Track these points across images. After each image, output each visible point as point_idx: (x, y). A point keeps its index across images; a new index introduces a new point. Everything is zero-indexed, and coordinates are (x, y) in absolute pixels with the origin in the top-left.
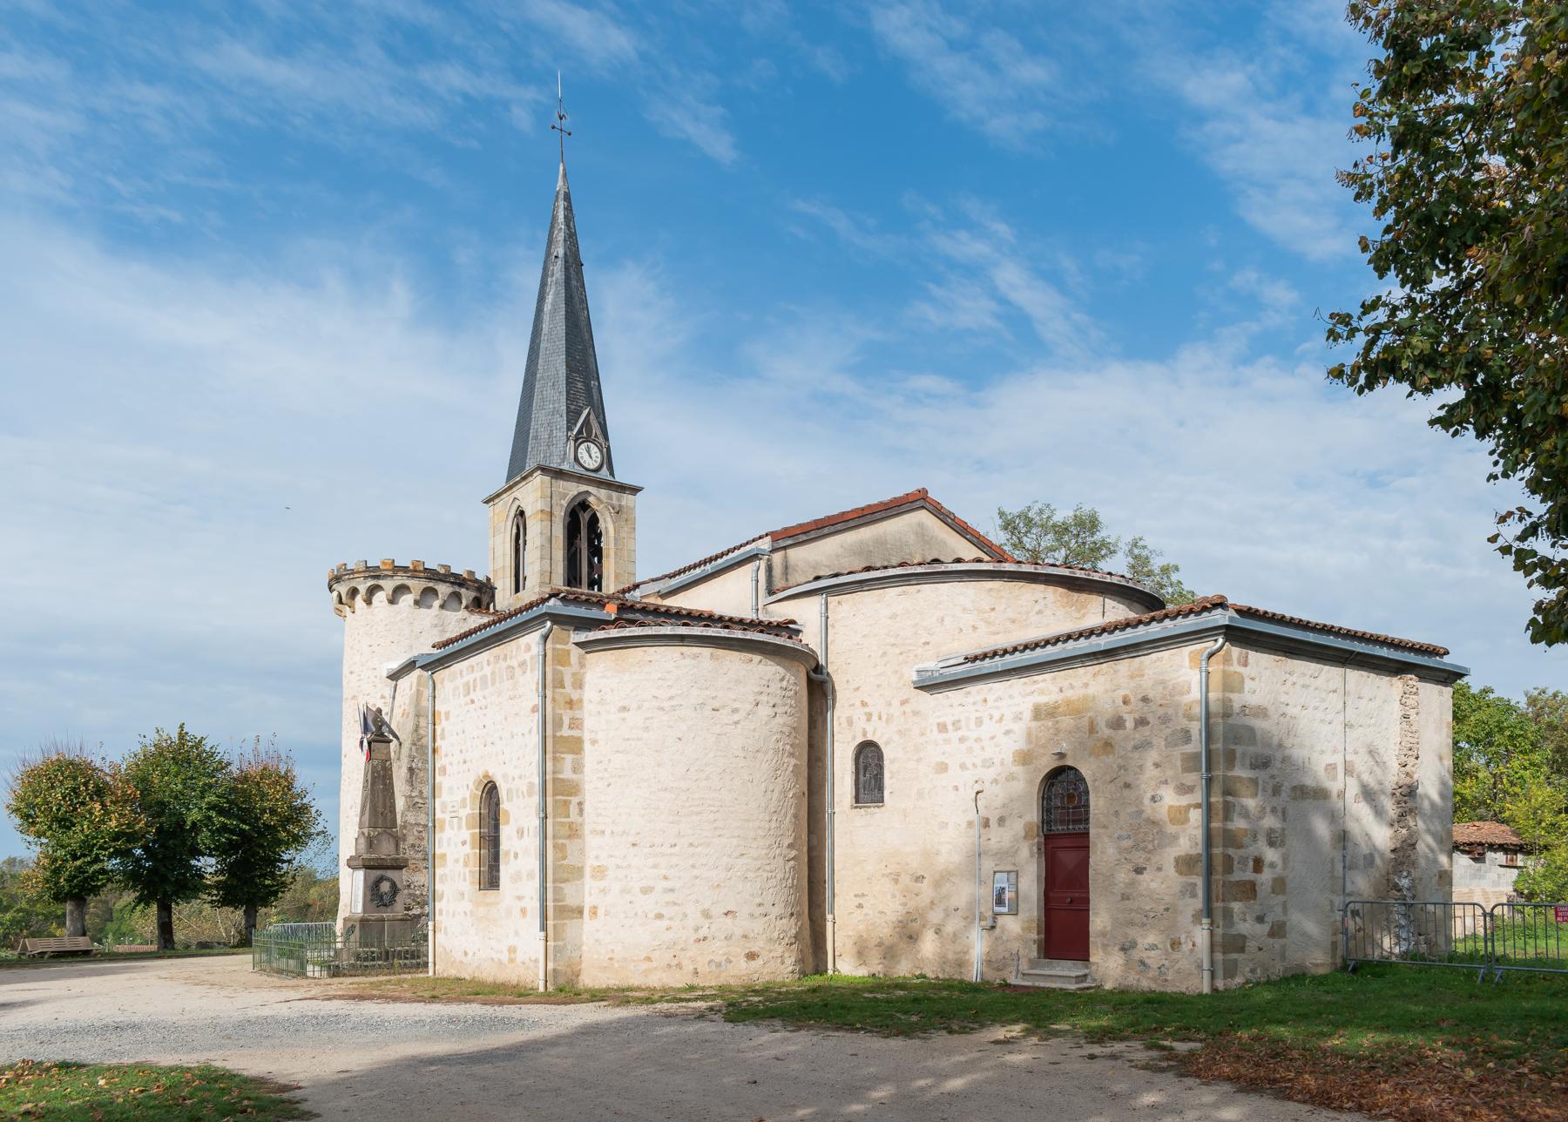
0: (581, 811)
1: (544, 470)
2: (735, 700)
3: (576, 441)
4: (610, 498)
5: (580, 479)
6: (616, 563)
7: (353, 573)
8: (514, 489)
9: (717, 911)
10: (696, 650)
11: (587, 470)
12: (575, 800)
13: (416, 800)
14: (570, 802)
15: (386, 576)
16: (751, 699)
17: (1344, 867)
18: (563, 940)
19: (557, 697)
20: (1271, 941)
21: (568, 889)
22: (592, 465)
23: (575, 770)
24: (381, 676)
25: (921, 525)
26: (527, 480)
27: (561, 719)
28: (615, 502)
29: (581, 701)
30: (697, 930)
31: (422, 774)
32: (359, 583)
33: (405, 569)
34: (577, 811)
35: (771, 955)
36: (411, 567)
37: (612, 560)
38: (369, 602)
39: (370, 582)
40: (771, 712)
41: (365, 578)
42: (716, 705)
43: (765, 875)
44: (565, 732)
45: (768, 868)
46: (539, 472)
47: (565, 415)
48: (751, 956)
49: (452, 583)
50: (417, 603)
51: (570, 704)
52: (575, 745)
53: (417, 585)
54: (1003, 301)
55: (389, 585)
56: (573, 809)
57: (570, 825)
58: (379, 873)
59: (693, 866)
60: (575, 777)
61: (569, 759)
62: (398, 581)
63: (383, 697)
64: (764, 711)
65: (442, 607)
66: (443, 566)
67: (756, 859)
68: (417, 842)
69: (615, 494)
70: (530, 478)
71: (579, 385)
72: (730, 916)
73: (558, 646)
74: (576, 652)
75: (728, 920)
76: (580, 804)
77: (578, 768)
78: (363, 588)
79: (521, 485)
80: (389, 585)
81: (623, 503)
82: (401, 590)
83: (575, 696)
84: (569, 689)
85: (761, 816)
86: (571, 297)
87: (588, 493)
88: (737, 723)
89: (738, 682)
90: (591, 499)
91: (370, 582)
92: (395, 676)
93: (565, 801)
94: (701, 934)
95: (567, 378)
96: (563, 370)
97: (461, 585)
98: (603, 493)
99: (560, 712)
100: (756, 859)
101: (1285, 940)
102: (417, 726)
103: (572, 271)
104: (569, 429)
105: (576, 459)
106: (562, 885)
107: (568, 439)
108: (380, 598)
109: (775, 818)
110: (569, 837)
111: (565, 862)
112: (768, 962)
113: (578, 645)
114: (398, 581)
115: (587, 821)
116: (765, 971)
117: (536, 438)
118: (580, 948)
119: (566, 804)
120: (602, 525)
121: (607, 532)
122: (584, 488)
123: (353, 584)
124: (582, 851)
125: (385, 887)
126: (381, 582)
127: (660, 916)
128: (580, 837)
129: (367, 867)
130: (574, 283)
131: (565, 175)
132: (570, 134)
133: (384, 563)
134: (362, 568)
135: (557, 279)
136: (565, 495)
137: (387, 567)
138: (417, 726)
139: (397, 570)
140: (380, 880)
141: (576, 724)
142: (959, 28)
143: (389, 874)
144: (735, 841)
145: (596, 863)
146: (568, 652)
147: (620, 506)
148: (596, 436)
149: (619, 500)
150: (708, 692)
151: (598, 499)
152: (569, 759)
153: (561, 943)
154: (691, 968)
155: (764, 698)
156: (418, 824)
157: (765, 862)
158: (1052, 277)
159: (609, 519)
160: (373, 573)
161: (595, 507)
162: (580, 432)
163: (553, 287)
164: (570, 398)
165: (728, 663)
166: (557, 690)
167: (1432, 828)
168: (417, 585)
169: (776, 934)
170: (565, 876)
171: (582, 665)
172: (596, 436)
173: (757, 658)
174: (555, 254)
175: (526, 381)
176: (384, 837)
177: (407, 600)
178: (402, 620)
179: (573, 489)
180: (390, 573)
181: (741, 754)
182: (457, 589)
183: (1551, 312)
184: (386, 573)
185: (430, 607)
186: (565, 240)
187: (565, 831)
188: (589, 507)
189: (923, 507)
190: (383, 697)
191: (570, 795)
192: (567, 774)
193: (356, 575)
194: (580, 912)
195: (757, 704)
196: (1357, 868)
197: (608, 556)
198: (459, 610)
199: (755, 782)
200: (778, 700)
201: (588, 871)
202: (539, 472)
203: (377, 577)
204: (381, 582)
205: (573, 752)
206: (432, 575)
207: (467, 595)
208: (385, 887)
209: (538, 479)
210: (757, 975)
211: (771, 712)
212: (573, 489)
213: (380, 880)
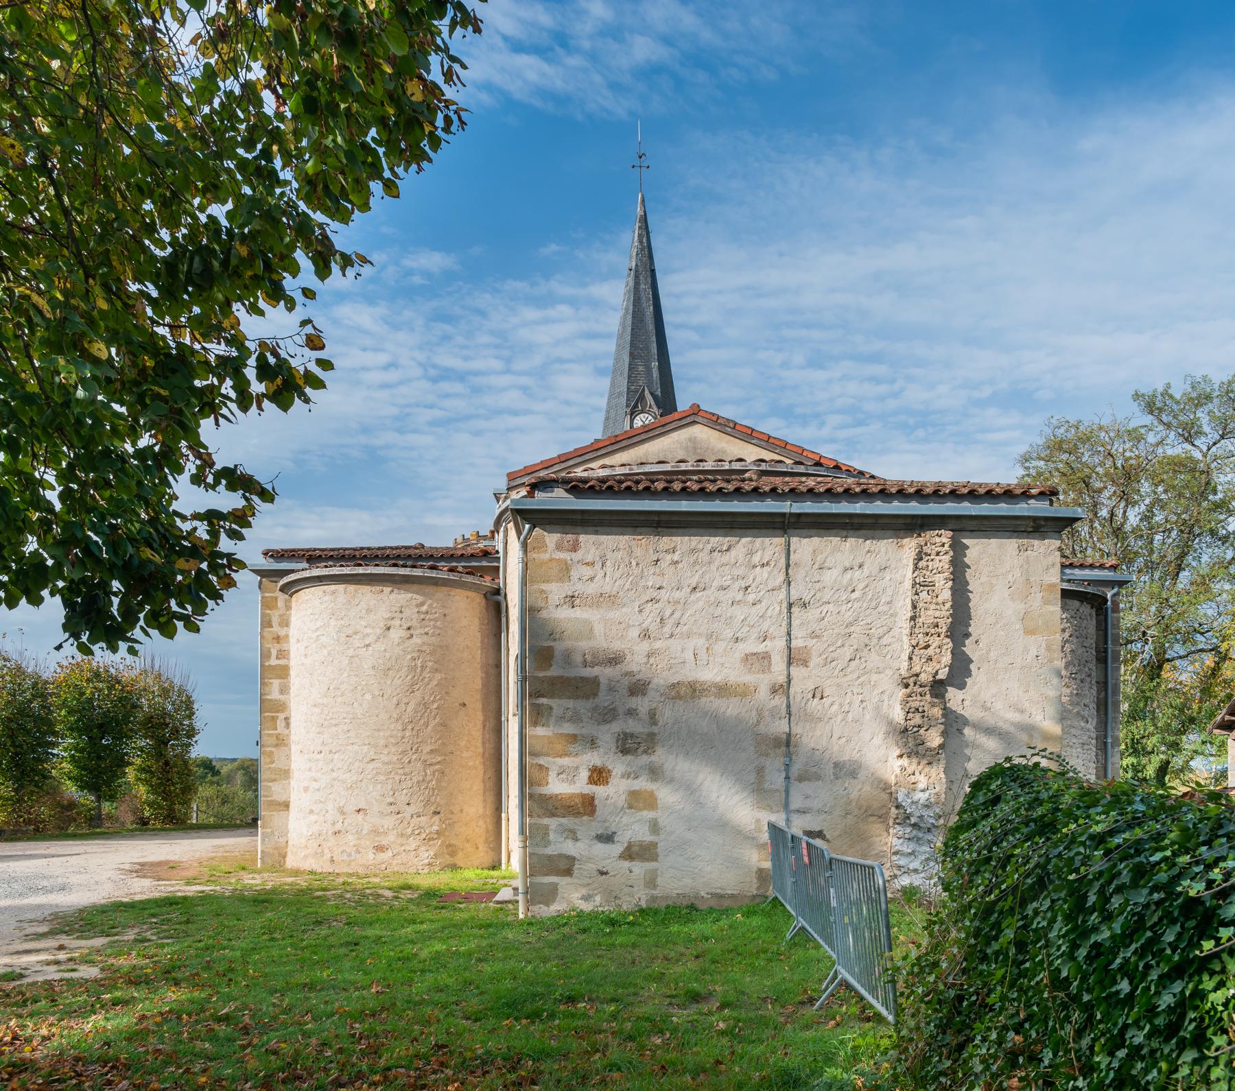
0: (288, 725)
2: (366, 627)
3: (631, 415)
9: (351, 808)
10: (333, 587)
12: (281, 716)
14: (277, 717)
16: (382, 624)
17: (787, 778)
18: (271, 828)
19: (265, 634)
20: (626, 864)
23: (282, 692)
25: (693, 440)
27: (270, 652)
29: (287, 636)
30: (334, 824)
34: (284, 724)
35: (403, 848)
40: (405, 634)
42: (350, 632)
43: (397, 778)
44: (273, 662)
45: (401, 771)
48: (380, 849)
51: (278, 639)
52: (283, 672)
56: (280, 724)
57: (278, 736)
59: (333, 770)
60: (282, 697)
61: (276, 683)
64: (396, 634)
67: (387, 763)
71: (641, 368)
72: (361, 813)
73: (267, 595)
74: (282, 597)
75: (360, 816)
76: (287, 719)
77: (284, 690)
83: (282, 632)
84: (276, 628)
85: (392, 726)
86: (639, 299)
88: (368, 645)
89: (369, 611)
93: (273, 717)
94: (338, 826)
95: (630, 364)
99: (268, 646)
100: (387, 763)
101: (654, 864)
103: (641, 278)
106: (270, 784)
109: (410, 727)
110: (277, 745)
111: (273, 765)
112: (398, 854)
113: (283, 589)
115: (293, 731)
116: (395, 862)
118: (286, 835)
119: (274, 719)
124: (288, 757)
127: (311, 812)
128: (286, 745)
131: (643, 201)
141: (283, 654)
144: (366, 748)
146: (276, 599)
148: (650, 407)
150: (343, 622)
152: (276, 683)
153: (269, 830)
154: (329, 856)
155: (397, 622)
157: (397, 766)
165: (360, 595)
166: (266, 629)
169: (409, 831)
170: (273, 777)
171: (288, 608)
172: (650, 407)
173: (387, 590)
181: (372, 673)
183: (312, 43)
186: (637, 254)
187: (273, 741)
189: (695, 422)
191: (278, 711)
192: (274, 694)
194: (286, 806)
195: (389, 629)
196: (818, 777)
199: (385, 697)
200: (414, 623)
205: (280, 677)
210: (384, 866)
211: (405, 634)
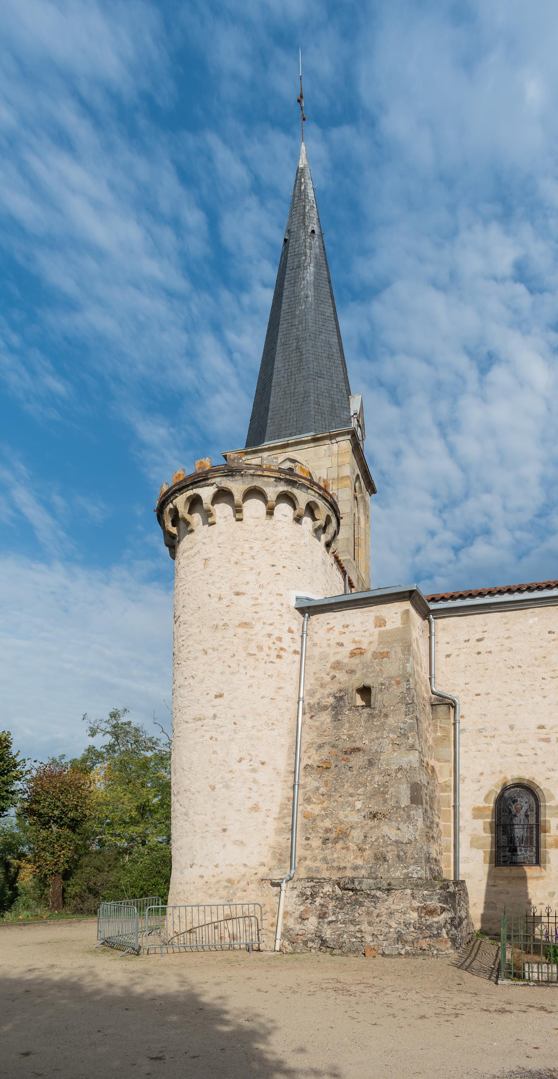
7: (263, 470)
8: (290, 449)
15: (303, 485)
24: (289, 607)
26: (321, 443)
32: (268, 484)
39: (283, 488)
41: (278, 479)
46: (349, 437)
54: (17, 511)
63: (290, 631)
70: (328, 442)
79: (306, 446)
80: (303, 497)
91: (283, 488)
123: (258, 483)
126: (296, 492)
135: (316, 255)
137: (304, 475)
142: (15, 340)
158: (49, 507)
180: (307, 483)
184: (303, 481)
193: (266, 473)
202: (349, 437)
204: (296, 492)
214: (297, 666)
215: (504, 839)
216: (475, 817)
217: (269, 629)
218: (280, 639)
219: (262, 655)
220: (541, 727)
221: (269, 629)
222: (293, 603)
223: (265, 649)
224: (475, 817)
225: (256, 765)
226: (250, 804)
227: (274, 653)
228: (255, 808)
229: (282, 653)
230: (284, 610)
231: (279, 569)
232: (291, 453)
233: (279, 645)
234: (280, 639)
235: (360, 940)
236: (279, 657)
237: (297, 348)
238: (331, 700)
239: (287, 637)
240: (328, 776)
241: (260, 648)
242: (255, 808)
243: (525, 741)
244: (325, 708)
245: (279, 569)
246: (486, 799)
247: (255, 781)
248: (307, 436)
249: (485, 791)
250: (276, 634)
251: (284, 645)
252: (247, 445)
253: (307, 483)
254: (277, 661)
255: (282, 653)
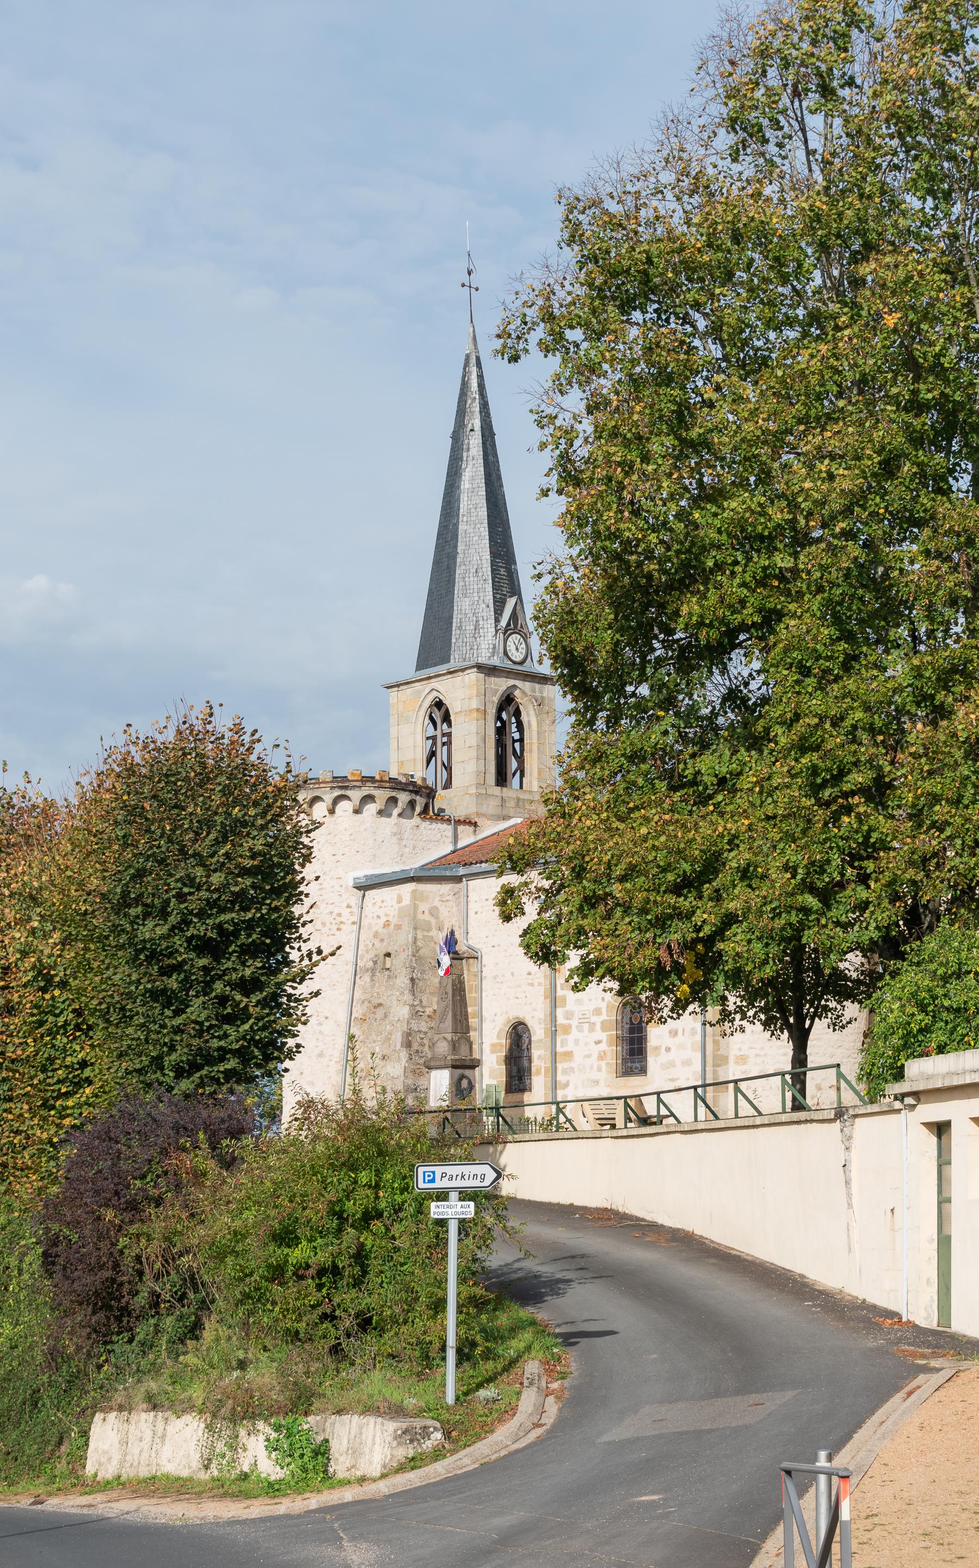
1: (480, 667)
4: (533, 690)
5: (509, 674)
6: (539, 758)
11: (514, 663)
13: (418, 1008)
21: (720, 1071)
22: (518, 657)
24: (347, 888)
28: (537, 694)
31: (421, 984)
32: (325, 793)
33: (372, 779)
36: (378, 778)
37: (535, 755)
38: (332, 811)
41: (332, 788)
47: (491, 606)
49: (411, 791)
50: (380, 813)
53: (382, 795)
55: (356, 795)
58: (460, 1071)
62: (365, 791)
63: (349, 906)
65: (400, 815)
66: (405, 775)
68: (420, 1048)
69: (537, 686)
71: (502, 571)
78: (329, 797)
80: (356, 795)
81: (545, 695)
82: (369, 798)
87: (515, 687)
90: (517, 693)
91: (337, 793)
92: (364, 887)
95: (492, 565)
96: (487, 556)
97: (416, 793)
98: (527, 686)
102: (415, 939)
104: (497, 620)
105: (506, 653)
107: (497, 631)
108: (345, 807)
114: (365, 791)
117: (460, 628)
120: (524, 718)
121: (530, 725)
122: (511, 682)
123: (317, 793)
125: (465, 1083)
126: (348, 793)
129: (454, 1067)
130: (491, 458)
132: (477, 289)
133: (353, 774)
134: (329, 778)
136: (496, 691)
138: (415, 939)
139: (367, 780)
140: (462, 1077)
143: (467, 1072)
145: (739, 1053)
147: (542, 698)
149: (541, 692)
151: (523, 692)
156: (420, 1031)
159: (532, 713)
160: (341, 783)
161: (519, 700)
162: (509, 624)
163: (471, 463)
164: (496, 588)
167: (738, 933)
168: (382, 795)
174: (470, 427)
175: (437, 563)
176: (463, 1041)
177: (371, 808)
178: (366, 830)
179: (501, 685)
180: (358, 784)
182: (414, 796)
185: (389, 816)
188: (513, 700)
190: (349, 906)
197: (531, 751)
198: (412, 817)
201: (732, 1060)
203: (346, 788)
204: (348, 793)
206: (396, 784)
207: (420, 802)
208: (465, 1083)
209: (473, 676)
212: (501, 685)
213: (462, 1077)
214: (354, 935)
215: (515, 1069)
216: (493, 1052)
217: (331, 908)
218: (340, 915)
219: (325, 930)
220: (529, 974)
221: (331, 908)
222: (351, 883)
223: (328, 925)
224: (493, 1052)
225: (322, 1019)
226: (317, 1052)
227: (335, 927)
228: (321, 1055)
229: (342, 926)
230: (342, 890)
231: (339, 857)
232: (434, 684)
233: (339, 919)
234: (340, 915)
235: (561, 1116)
236: (339, 929)
237: (448, 567)
238: (371, 964)
239: (346, 912)
240: (365, 1026)
241: (324, 924)
242: (321, 1055)
243: (519, 986)
244: (367, 970)
245: (339, 857)
246: (498, 1037)
247: (321, 1032)
248: (442, 669)
249: (497, 1029)
250: (337, 911)
251: (342, 919)
252: (421, 665)
253: (358, 784)
254: (337, 933)
255: (342, 926)
